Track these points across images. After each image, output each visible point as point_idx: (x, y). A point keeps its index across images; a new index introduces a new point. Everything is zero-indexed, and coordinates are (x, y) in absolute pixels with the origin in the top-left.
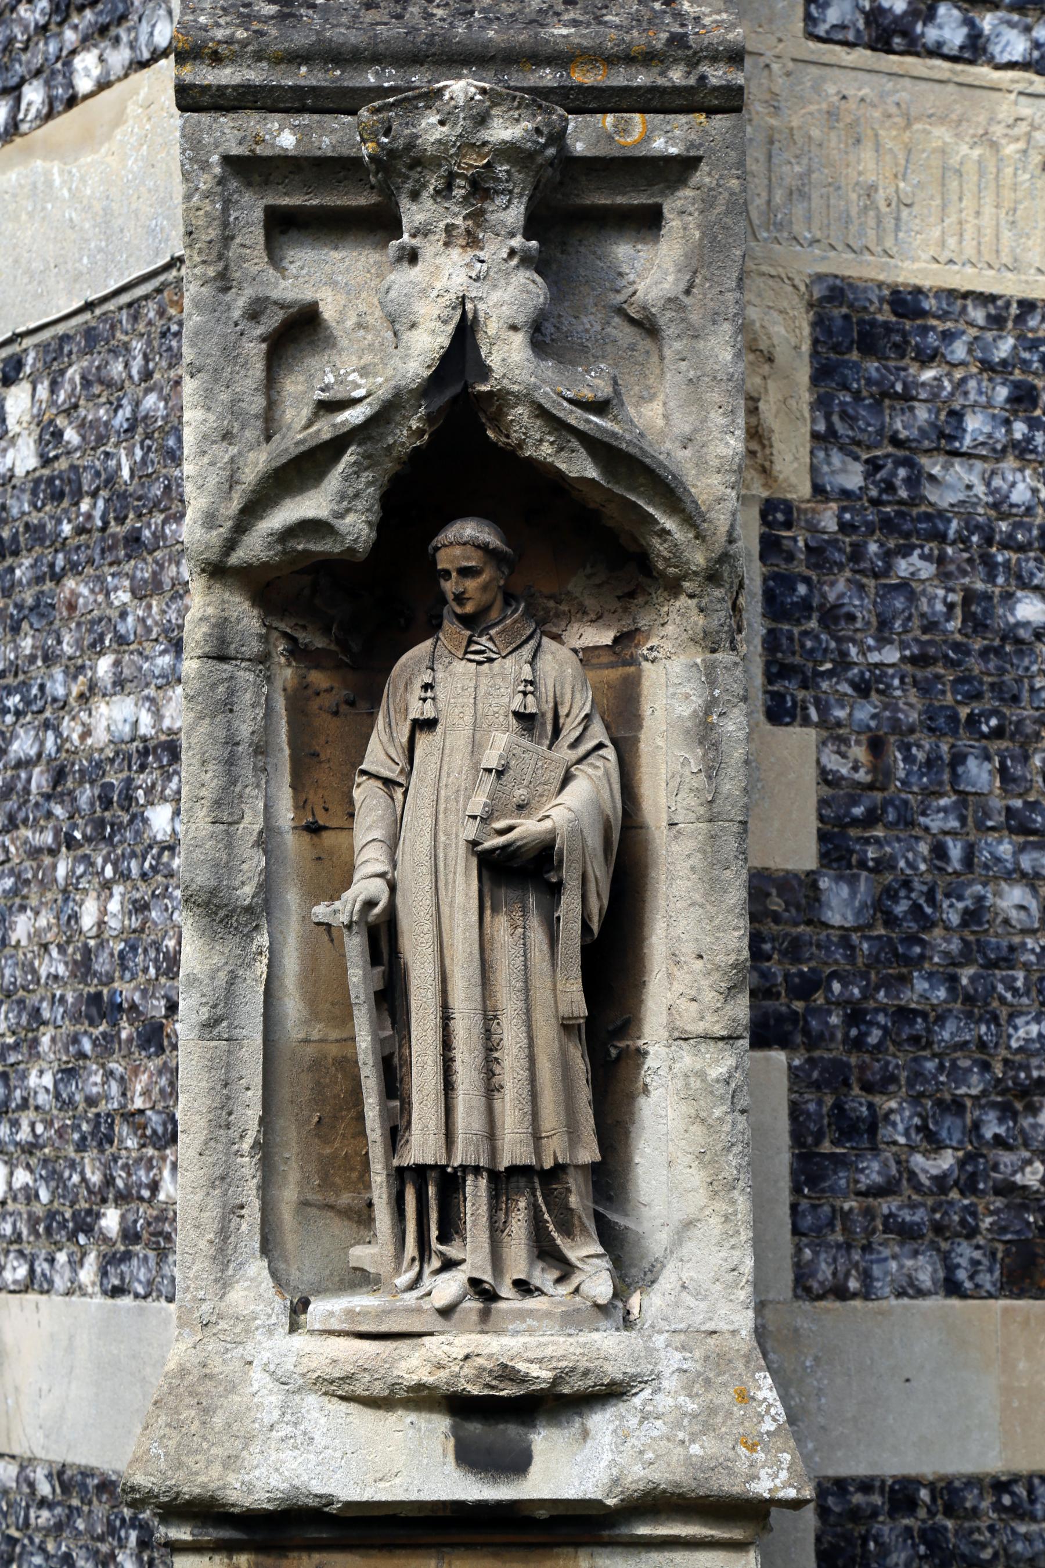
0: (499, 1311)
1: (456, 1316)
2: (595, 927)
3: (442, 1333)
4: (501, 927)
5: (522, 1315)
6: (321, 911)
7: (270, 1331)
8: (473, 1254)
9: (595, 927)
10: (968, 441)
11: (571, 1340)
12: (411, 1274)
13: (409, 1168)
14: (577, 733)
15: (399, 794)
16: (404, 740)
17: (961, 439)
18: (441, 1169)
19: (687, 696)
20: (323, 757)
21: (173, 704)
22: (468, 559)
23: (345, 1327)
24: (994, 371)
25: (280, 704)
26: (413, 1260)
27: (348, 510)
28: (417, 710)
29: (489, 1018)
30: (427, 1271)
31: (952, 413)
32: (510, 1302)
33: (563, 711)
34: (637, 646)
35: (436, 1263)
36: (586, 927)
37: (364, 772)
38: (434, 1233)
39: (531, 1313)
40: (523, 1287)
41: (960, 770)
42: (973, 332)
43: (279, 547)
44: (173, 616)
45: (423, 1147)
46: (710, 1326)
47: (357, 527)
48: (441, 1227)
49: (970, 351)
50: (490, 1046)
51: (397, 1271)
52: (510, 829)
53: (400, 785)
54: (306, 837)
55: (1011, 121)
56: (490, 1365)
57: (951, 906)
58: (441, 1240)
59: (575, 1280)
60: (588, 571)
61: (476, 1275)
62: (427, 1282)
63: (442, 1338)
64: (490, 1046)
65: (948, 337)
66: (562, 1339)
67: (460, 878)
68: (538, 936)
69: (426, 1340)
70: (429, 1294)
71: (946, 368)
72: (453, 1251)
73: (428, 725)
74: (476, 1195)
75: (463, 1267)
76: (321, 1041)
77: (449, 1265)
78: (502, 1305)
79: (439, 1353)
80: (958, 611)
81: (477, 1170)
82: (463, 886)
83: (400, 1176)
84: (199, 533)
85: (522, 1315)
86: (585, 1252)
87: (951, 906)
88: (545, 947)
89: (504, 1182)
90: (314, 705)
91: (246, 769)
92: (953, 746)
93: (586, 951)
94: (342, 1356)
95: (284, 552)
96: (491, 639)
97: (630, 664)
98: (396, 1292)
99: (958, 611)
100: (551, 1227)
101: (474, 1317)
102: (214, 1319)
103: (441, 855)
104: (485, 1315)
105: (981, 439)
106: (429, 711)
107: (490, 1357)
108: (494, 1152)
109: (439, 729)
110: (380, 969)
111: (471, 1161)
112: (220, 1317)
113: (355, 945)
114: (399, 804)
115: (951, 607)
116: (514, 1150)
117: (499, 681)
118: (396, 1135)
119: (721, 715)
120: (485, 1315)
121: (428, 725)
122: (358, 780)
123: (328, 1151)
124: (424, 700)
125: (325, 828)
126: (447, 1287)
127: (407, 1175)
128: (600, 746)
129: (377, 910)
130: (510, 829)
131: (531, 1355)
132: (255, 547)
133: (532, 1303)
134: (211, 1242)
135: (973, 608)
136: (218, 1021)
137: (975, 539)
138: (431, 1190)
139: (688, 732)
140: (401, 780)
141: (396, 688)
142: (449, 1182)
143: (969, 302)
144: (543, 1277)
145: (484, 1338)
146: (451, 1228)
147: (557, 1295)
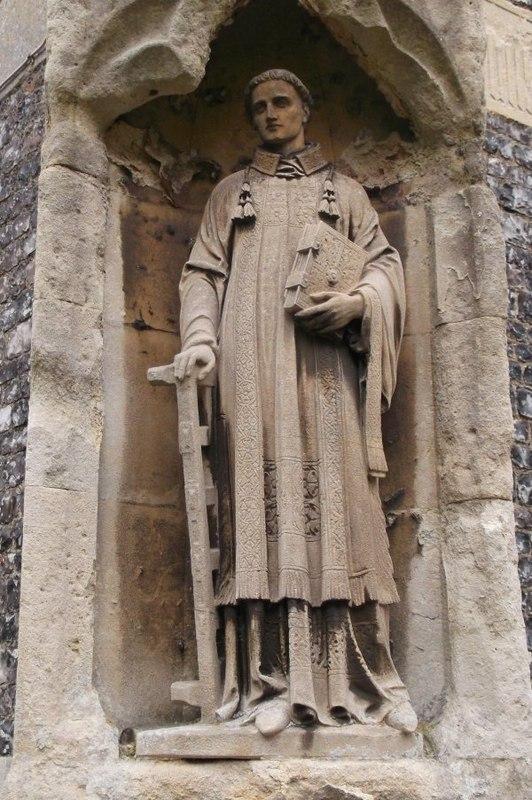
0: (319, 736)
1: (281, 741)
2: (389, 399)
3: (268, 758)
4: (314, 387)
5: (343, 740)
6: (156, 372)
7: (103, 755)
8: (300, 685)
9: (389, 399)
10: (516, 204)
11: (387, 765)
12: (231, 705)
13: (230, 605)
14: (370, 239)
15: (220, 285)
16: (225, 241)
17: (512, 202)
18: (266, 603)
19: (451, 222)
20: (149, 271)
21: (15, 338)
22: (282, 90)
23: (175, 751)
24: (526, 167)
25: (116, 222)
26: (233, 691)
27: (185, 41)
28: (236, 212)
29: (310, 466)
30: (246, 702)
31: (506, 186)
32: (329, 729)
33: (356, 223)
34: (401, 195)
35: (256, 694)
36: (384, 400)
37: (190, 267)
38: (256, 663)
39: (351, 738)
40: (340, 714)
41: (524, 403)
42: (514, 143)
43: (124, 79)
44: (18, 281)
45: (248, 583)
46: (499, 754)
47: (193, 58)
48: (264, 657)
49: (514, 153)
50: (311, 493)
51: (218, 703)
52: (326, 299)
53: (222, 275)
54: (134, 333)
55: (524, 33)
56: (315, 788)
57: (523, 489)
58: (265, 669)
59: (385, 709)
60: (358, 142)
61: (301, 701)
62: (248, 712)
63: (267, 763)
64: (311, 493)
65: (501, 142)
66: (379, 764)
67: (280, 344)
68: (347, 397)
69: (254, 764)
70: (253, 721)
71: (501, 160)
72: (274, 681)
73: (246, 223)
74: (299, 624)
75: (284, 696)
76: (143, 504)
77: (270, 694)
78: (322, 731)
79: (266, 777)
80: (516, 304)
81: (300, 603)
82: (285, 351)
83: (221, 611)
84: (59, 69)
85: (343, 740)
86: (390, 684)
87: (523, 489)
88: (353, 408)
89: (326, 614)
90: (144, 229)
91: (93, 262)
92: (518, 387)
93: (385, 417)
94: (174, 780)
95: (129, 83)
96: (298, 162)
97: (395, 209)
98: (218, 720)
99: (516, 304)
100: (362, 660)
101: (297, 742)
102: (49, 743)
103: (263, 326)
104: (308, 742)
105: (523, 204)
106: (249, 211)
107: (316, 780)
108: (316, 589)
109: (258, 225)
110: (205, 428)
111: (294, 594)
112: (56, 741)
113: (188, 399)
114: (220, 297)
115: (512, 300)
116: (336, 585)
117: (307, 191)
118: (221, 575)
119: (485, 231)
120: (308, 742)
121: (246, 223)
122: (184, 274)
123: (148, 600)
124: (243, 205)
125: (150, 328)
126: (273, 715)
127: (228, 613)
128: (387, 251)
129: (207, 369)
130: (326, 299)
131: (353, 778)
132: (103, 82)
133: (350, 730)
134: (49, 671)
135: (525, 304)
136: (62, 470)
137: (522, 262)
138: (254, 624)
139: (453, 248)
140: (223, 271)
141: (215, 202)
142: (275, 612)
143: (510, 125)
144: (356, 706)
145: (309, 763)
146: (276, 659)
147: (367, 725)
